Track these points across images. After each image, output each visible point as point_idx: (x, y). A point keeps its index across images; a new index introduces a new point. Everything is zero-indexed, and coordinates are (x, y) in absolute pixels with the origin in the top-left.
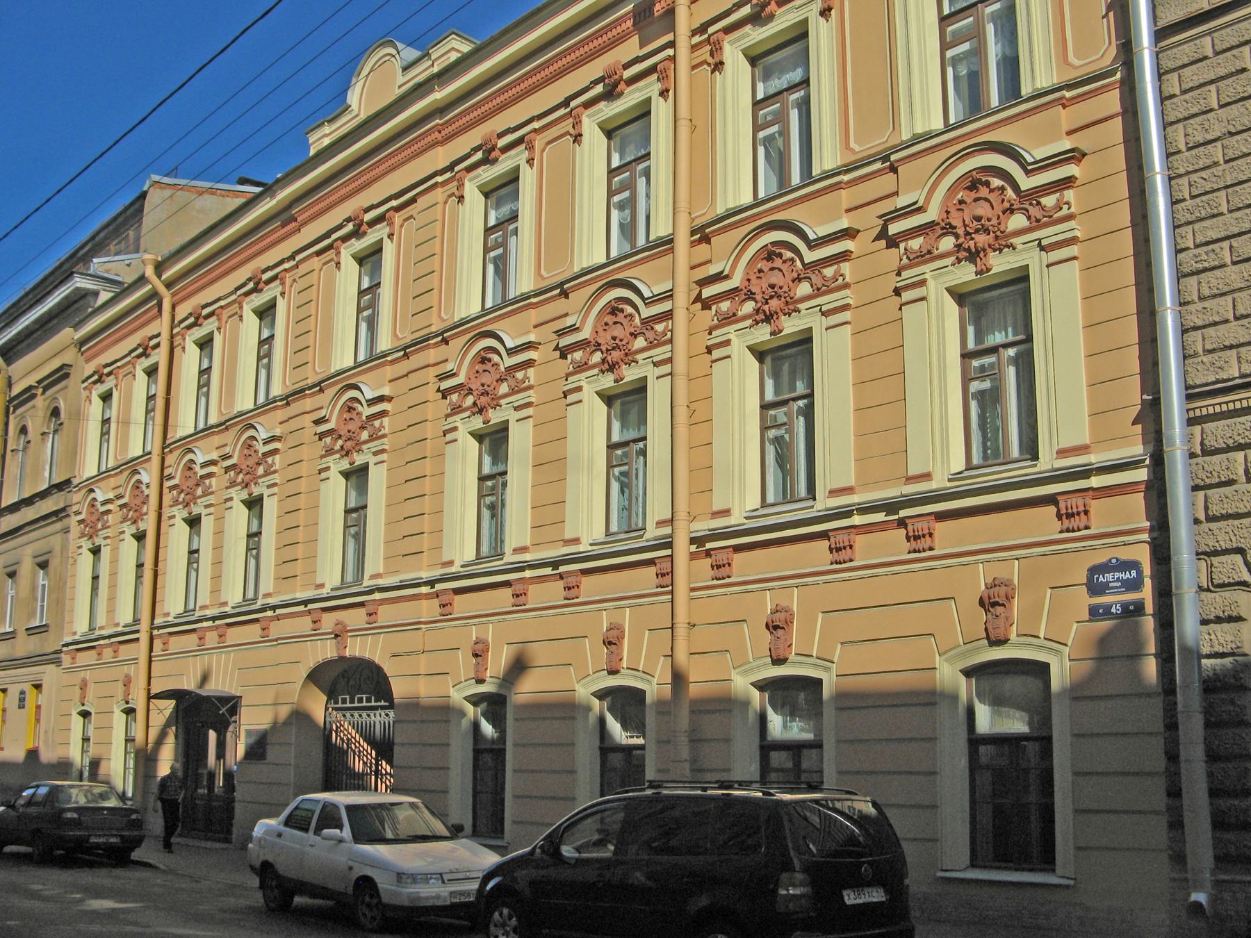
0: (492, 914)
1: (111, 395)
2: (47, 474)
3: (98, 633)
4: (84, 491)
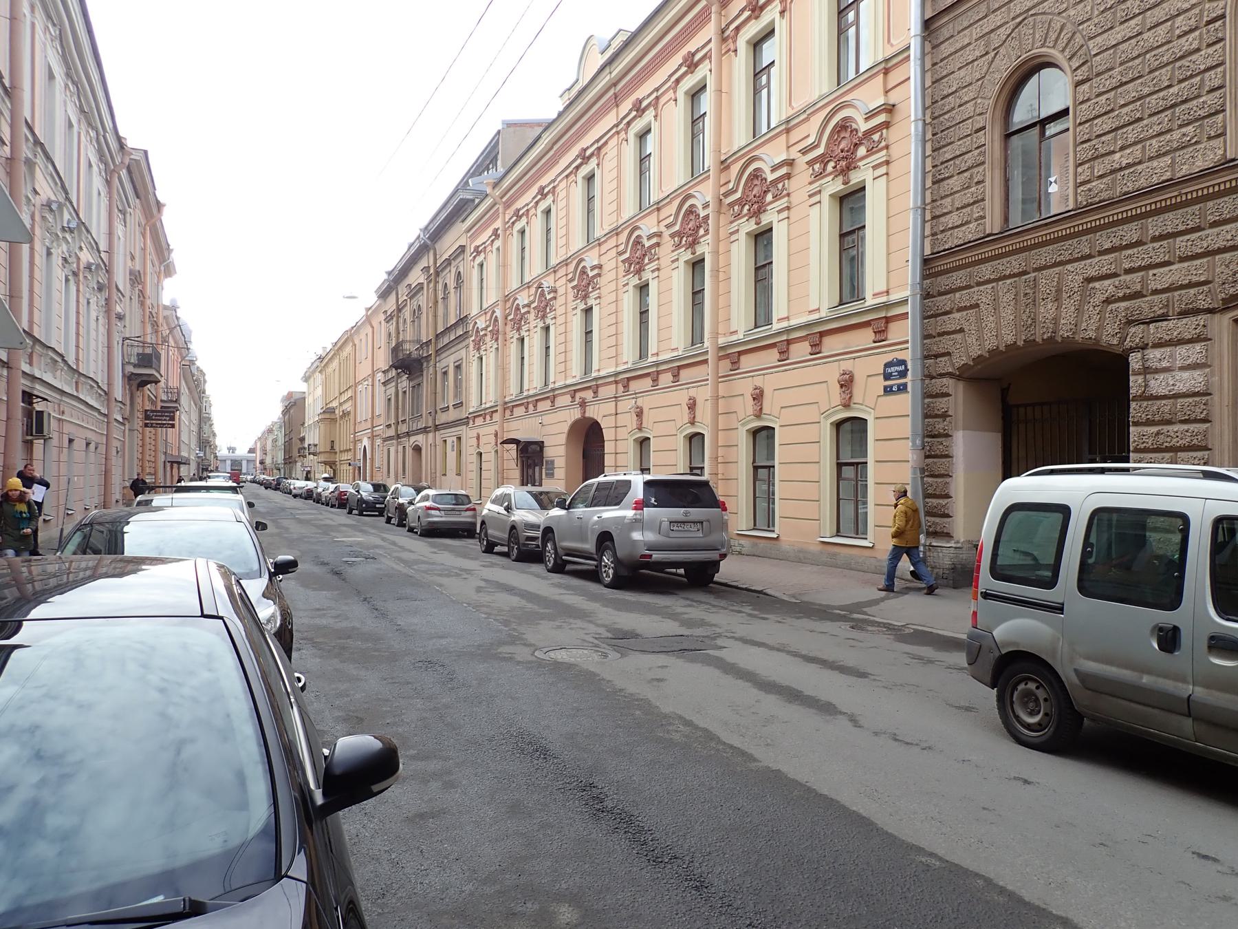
1: (550, 210)
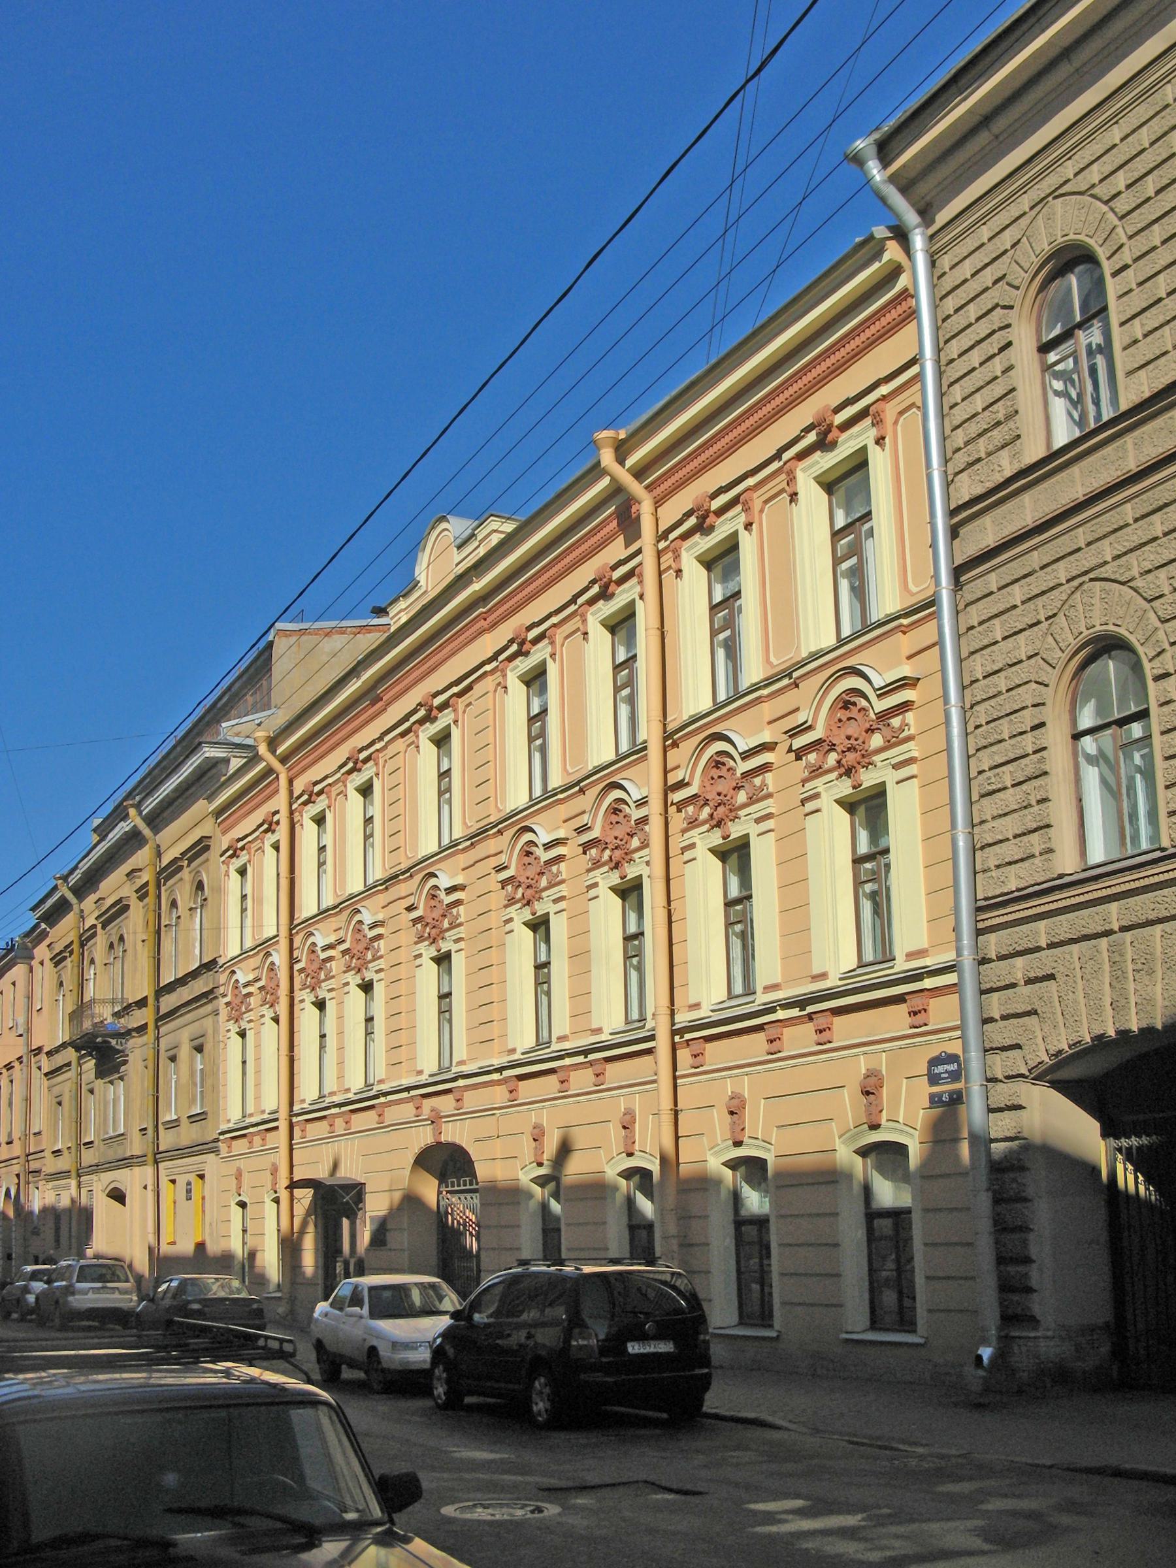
0: (534, 1383)
2: (197, 952)
3: (249, 1120)
4: (346, 913)
